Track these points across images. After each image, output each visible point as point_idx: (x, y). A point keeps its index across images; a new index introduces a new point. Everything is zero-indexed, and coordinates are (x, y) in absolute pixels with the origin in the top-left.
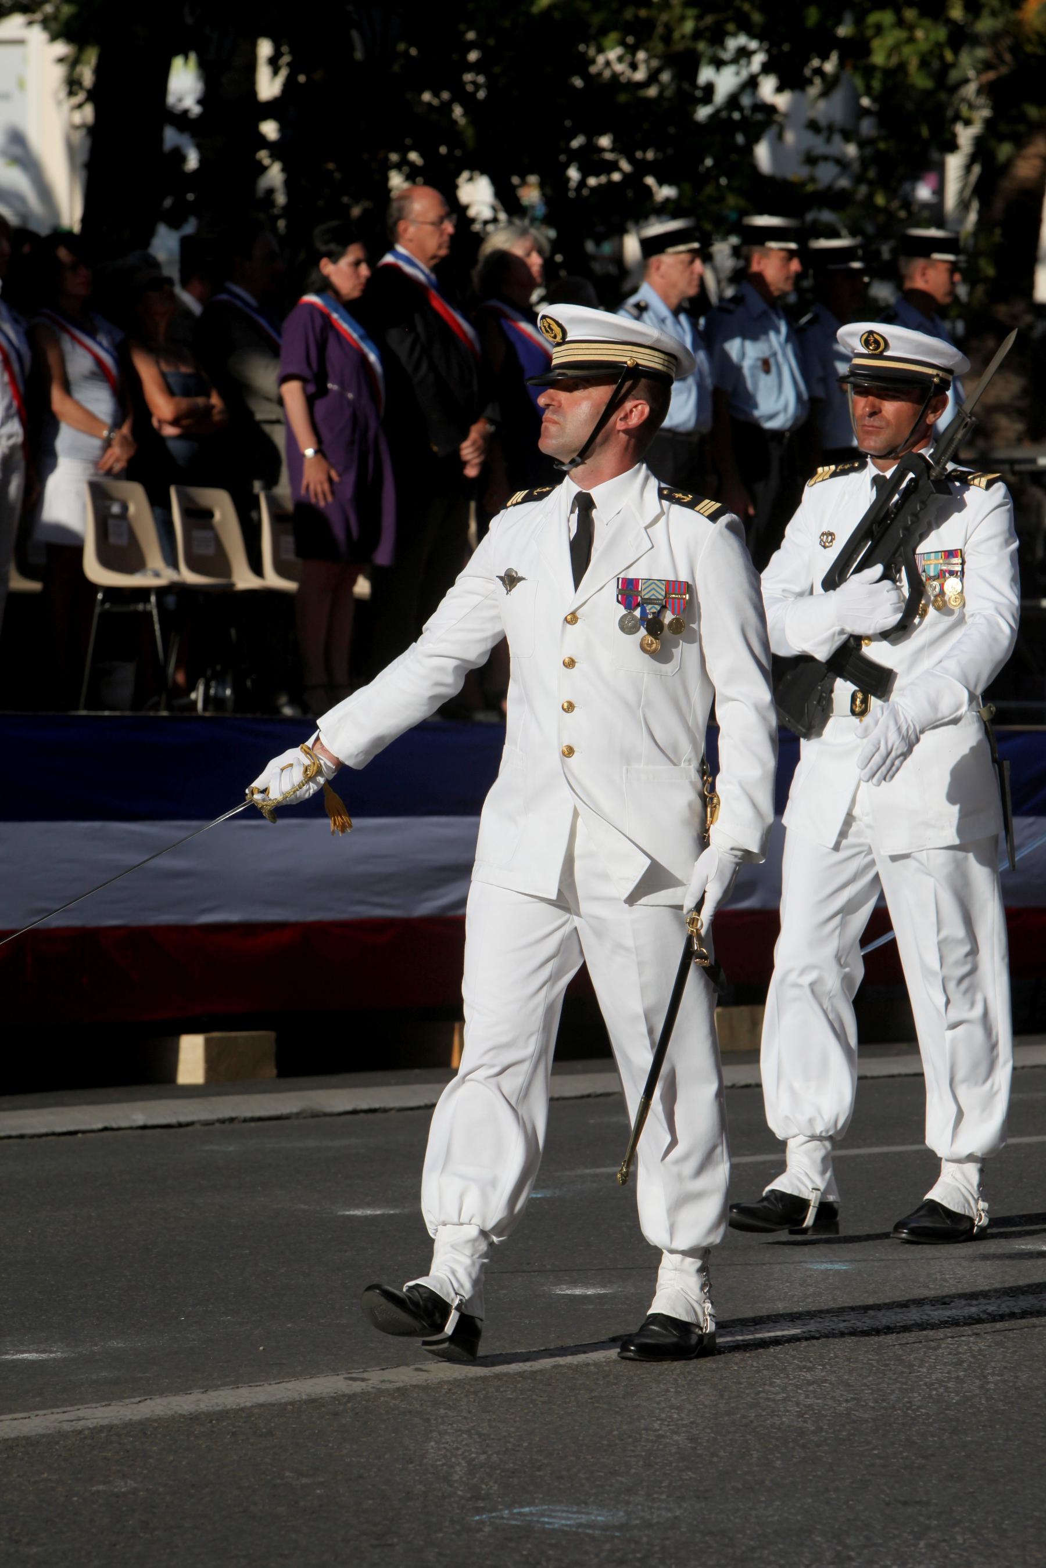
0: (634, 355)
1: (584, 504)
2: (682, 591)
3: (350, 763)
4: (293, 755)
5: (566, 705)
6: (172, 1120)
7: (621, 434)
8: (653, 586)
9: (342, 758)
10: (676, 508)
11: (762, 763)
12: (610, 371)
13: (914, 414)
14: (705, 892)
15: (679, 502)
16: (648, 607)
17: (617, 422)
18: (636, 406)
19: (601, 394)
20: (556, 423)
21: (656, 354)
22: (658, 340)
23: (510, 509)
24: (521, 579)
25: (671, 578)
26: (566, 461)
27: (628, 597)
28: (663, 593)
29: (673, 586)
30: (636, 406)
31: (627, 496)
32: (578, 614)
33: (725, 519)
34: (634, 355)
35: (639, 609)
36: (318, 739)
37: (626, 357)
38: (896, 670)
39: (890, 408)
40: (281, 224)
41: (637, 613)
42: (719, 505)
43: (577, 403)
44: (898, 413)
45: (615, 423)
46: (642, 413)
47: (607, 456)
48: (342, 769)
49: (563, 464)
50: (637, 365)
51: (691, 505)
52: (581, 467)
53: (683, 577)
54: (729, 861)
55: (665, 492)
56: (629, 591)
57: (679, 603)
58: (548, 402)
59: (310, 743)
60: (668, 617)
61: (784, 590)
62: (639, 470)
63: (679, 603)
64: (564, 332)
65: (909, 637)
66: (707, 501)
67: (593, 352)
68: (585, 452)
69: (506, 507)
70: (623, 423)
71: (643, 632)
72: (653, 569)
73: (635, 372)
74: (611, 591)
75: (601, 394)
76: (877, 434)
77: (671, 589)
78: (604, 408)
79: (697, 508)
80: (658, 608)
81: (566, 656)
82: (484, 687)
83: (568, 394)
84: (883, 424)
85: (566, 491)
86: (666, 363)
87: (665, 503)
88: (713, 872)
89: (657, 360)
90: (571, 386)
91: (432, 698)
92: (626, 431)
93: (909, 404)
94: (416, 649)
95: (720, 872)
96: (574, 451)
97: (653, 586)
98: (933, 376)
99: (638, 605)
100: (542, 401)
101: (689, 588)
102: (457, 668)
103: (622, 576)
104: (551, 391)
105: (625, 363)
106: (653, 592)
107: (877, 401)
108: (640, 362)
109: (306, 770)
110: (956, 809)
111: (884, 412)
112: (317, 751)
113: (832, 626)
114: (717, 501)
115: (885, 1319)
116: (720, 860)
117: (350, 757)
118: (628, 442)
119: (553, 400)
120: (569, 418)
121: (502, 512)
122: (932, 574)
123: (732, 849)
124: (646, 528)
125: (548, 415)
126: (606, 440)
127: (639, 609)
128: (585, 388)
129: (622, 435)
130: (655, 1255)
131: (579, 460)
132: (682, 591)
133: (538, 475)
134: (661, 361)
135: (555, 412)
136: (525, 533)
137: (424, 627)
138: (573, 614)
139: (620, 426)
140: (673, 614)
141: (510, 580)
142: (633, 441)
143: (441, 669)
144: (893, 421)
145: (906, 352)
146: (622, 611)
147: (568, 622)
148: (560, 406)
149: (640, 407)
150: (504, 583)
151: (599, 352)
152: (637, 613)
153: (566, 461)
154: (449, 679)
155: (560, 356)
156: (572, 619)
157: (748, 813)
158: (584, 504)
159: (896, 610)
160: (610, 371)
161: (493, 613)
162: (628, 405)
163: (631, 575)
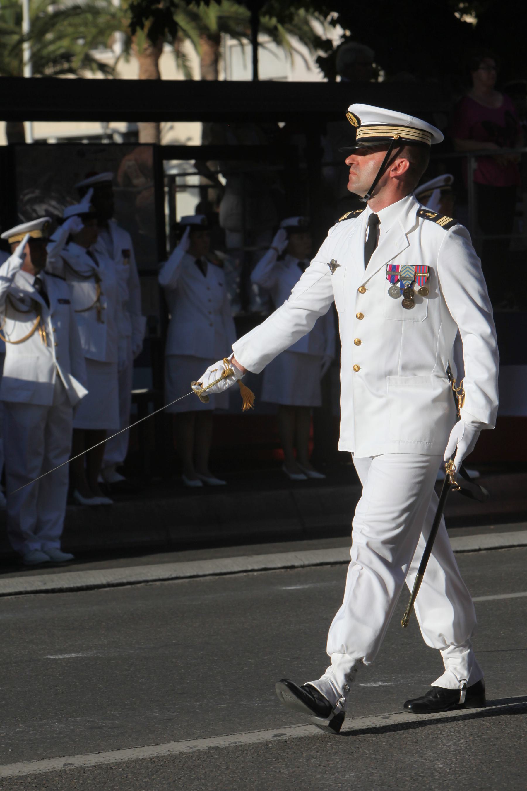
0: (399, 132)
1: (374, 222)
2: (425, 271)
3: (250, 369)
4: (219, 365)
5: (356, 341)
7: (394, 179)
8: (408, 269)
9: (245, 366)
10: (427, 221)
11: (488, 370)
12: (386, 142)
14: (457, 448)
15: (428, 218)
16: (404, 282)
17: (390, 172)
18: (402, 162)
19: (379, 156)
20: (355, 174)
21: (414, 130)
22: (411, 123)
23: (341, 222)
24: (338, 266)
25: (420, 264)
26: (363, 196)
27: (392, 276)
28: (414, 273)
29: (418, 269)
30: (402, 162)
31: (398, 217)
32: (366, 287)
33: (453, 228)
34: (399, 132)
35: (399, 283)
36: (233, 357)
37: (393, 133)
41: (399, 285)
42: (452, 219)
43: (366, 162)
45: (389, 173)
46: (405, 166)
47: (387, 192)
48: (246, 372)
49: (362, 198)
50: (400, 138)
51: (435, 220)
52: (372, 200)
53: (427, 264)
54: (471, 429)
55: (421, 213)
56: (393, 273)
57: (423, 279)
58: (351, 162)
59: (229, 358)
60: (417, 288)
62: (407, 200)
63: (423, 279)
64: (359, 121)
66: (445, 217)
67: (374, 131)
68: (373, 190)
69: (339, 222)
70: (394, 173)
71: (402, 297)
72: (410, 258)
73: (400, 142)
74: (383, 273)
75: (379, 156)
77: (418, 271)
78: (381, 164)
79: (438, 222)
80: (410, 282)
81: (358, 312)
82: (326, 325)
83: (363, 157)
85: (368, 212)
86: (421, 136)
87: (420, 219)
88: (461, 436)
89: (414, 134)
90: (364, 152)
91: (294, 333)
92: (396, 177)
94: (287, 304)
95: (465, 437)
96: (366, 191)
97: (408, 269)
99: (398, 281)
100: (348, 161)
101: (430, 270)
102: (308, 316)
103: (390, 263)
104: (353, 156)
105: (393, 137)
106: (408, 273)
108: (402, 136)
109: (224, 372)
110: (342, 446)
112: (233, 362)
114: (451, 218)
116: (466, 429)
117: (250, 366)
118: (399, 185)
119: (353, 160)
120: (363, 170)
121: (337, 224)
123: (473, 422)
124: (406, 235)
125: (352, 170)
126: (385, 183)
127: (399, 283)
128: (371, 153)
129: (394, 179)
130: (437, 652)
131: (369, 196)
132: (425, 271)
133: (354, 204)
134: (417, 135)
135: (355, 168)
136: (344, 236)
137: (292, 290)
138: (363, 287)
139: (392, 174)
140: (419, 285)
141: (333, 266)
142: (402, 183)
143: (299, 316)
146: (389, 285)
147: (360, 292)
148: (358, 164)
149: (404, 163)
150: (330, 266)
151: (377, 131)
152: (399, 285)
153: (363, 196)
154: (304, 322)
155: (360, 134)
156: (362, 290)
157: (482, 401)
158: (374, 222)
160: (386, 142)
161: (329, 284)
162: (397, 162)
163: (396, 263)
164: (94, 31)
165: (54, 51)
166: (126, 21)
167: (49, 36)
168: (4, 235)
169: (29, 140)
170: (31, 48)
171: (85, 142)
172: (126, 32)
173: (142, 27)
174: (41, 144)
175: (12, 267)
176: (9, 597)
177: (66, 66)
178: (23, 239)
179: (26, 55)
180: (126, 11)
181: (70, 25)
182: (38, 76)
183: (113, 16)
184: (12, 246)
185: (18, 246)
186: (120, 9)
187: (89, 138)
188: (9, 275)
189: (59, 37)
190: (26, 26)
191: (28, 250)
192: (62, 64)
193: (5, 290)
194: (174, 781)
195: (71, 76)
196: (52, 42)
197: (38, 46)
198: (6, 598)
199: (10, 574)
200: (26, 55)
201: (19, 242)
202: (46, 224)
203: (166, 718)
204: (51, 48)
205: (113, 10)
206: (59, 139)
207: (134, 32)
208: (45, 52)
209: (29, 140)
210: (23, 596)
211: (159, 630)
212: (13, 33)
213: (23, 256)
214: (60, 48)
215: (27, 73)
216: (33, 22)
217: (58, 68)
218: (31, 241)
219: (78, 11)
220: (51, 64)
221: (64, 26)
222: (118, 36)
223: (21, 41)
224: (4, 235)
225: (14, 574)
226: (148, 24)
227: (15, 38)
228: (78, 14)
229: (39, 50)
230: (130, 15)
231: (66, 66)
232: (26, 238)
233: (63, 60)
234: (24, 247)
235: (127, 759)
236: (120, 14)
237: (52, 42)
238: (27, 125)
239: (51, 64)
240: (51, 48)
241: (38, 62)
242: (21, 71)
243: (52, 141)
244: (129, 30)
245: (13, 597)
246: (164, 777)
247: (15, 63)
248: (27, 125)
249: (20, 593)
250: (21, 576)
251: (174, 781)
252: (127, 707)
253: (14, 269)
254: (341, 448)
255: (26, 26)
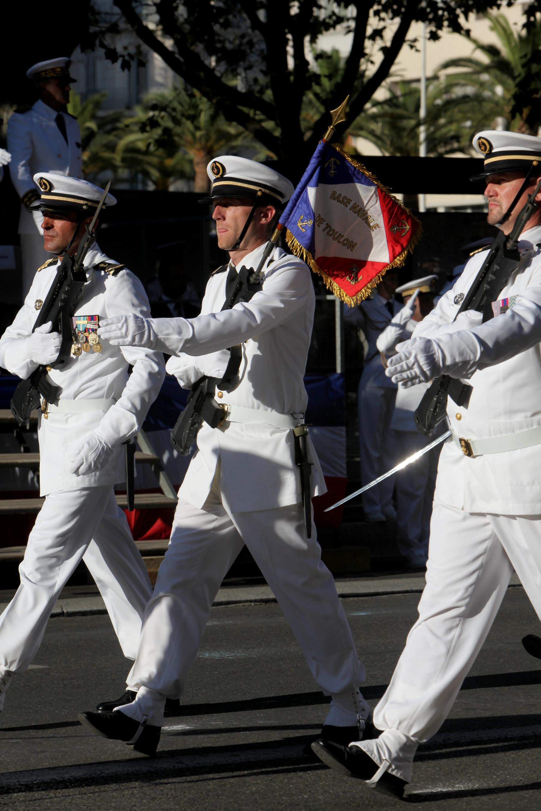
6: (372, 591)
13: (73, 228)
38: (62, 386)
39: (58, 224)
40: (292, 78)
44: (63, 229)
61: (18, 334)
64: (491, 147)
65: (70, 368)
76: (52, 240)
84: (55, 234)
93: (69, 222)
98: (83, 205)
107: (50, 220)
111: (55, 228)
113: (25, 360)
115: (189, 762)
122: (81, 330)
133: (220, 260)
144: (60, 233)
145: (63, 190)
159: (57, 351)
164: (479, 116)
165: (446, 134)
166: (508, 109)
167: (442, 121)
168: (398, 290)
169: (422, 210)
170: (427, 130)
171: (469, 211)
172: (507, 119)
173: (521, 114)
174: (432, 212)
175: (404, 317)
176: (398, 595)
177: (456, 145)
178: (413, 293)
179: (422, 137)
180: (509, 100)
181: (460, 111)
182: (432, 155)
183: (497, 104)
184: (405, 299)
185: (409, 299)
186: (503, 98)
187: (473, 207)
188: (402, 323)
189: (450, 122)
190: (422, 113)
191: (417, 303)
192: (452, 144)
193: (398, 336)
194: (537, 758)
195: (459, 155)
196: (444, 126)
197: (432, 129)
198: (395, 595)
199: (398, 575)
200: (422, 137)
201: (410, 296)
202: (433, 281)
203: (530, 704)
204: (444, 130)
205: (496, 99)
206: (447, 208)
207: (513, 117)
208: (438, 134)
209: (422, 210)
210: (410, 594)
211: (524, 627)
212: (410, 118)
213: (413, 308)
214: (450, 131)
215: (422, 153)
216: (428, 111)
217: (448, 148)
218: (420, 294)
219: (467, 100)
220: (442, 144)
221: (456, 112)
222: (500, 121)
223: (418, 125)
224: (398, 290)
225: (402, 575)
226: (526, 111)
227: (413, 122)
228: (466, 102)
229: (433, 133)
230: (513, 103)
231: (456, 145)
232: (416, 292)
233: (453, 140)
234: (415, 300)
235: (497, 737)
236: (502, 102)
237: (444, 126)
238: (421, 197)
239: (442, 144)
240: (444, 130)
241: (432, 142)
242: (417, 150)
243: (441, 210)
244: (509, 116)
245: (401, 595)
246: (528, 754)
247: (412, 144)
248: (421, 197)
249: (407, 592)
250: (408, 577)
251: (537, 758)
252: (497, 693)
253: (405, 318)
254: (22, 374)
255: (422, 113)
